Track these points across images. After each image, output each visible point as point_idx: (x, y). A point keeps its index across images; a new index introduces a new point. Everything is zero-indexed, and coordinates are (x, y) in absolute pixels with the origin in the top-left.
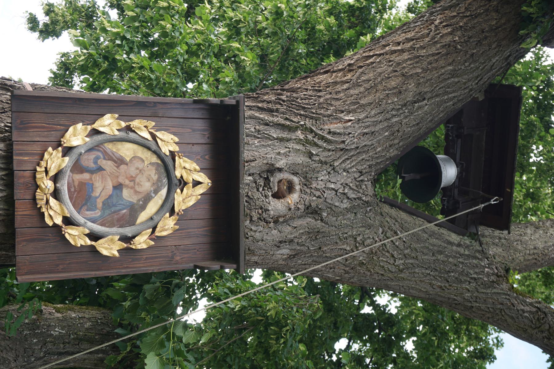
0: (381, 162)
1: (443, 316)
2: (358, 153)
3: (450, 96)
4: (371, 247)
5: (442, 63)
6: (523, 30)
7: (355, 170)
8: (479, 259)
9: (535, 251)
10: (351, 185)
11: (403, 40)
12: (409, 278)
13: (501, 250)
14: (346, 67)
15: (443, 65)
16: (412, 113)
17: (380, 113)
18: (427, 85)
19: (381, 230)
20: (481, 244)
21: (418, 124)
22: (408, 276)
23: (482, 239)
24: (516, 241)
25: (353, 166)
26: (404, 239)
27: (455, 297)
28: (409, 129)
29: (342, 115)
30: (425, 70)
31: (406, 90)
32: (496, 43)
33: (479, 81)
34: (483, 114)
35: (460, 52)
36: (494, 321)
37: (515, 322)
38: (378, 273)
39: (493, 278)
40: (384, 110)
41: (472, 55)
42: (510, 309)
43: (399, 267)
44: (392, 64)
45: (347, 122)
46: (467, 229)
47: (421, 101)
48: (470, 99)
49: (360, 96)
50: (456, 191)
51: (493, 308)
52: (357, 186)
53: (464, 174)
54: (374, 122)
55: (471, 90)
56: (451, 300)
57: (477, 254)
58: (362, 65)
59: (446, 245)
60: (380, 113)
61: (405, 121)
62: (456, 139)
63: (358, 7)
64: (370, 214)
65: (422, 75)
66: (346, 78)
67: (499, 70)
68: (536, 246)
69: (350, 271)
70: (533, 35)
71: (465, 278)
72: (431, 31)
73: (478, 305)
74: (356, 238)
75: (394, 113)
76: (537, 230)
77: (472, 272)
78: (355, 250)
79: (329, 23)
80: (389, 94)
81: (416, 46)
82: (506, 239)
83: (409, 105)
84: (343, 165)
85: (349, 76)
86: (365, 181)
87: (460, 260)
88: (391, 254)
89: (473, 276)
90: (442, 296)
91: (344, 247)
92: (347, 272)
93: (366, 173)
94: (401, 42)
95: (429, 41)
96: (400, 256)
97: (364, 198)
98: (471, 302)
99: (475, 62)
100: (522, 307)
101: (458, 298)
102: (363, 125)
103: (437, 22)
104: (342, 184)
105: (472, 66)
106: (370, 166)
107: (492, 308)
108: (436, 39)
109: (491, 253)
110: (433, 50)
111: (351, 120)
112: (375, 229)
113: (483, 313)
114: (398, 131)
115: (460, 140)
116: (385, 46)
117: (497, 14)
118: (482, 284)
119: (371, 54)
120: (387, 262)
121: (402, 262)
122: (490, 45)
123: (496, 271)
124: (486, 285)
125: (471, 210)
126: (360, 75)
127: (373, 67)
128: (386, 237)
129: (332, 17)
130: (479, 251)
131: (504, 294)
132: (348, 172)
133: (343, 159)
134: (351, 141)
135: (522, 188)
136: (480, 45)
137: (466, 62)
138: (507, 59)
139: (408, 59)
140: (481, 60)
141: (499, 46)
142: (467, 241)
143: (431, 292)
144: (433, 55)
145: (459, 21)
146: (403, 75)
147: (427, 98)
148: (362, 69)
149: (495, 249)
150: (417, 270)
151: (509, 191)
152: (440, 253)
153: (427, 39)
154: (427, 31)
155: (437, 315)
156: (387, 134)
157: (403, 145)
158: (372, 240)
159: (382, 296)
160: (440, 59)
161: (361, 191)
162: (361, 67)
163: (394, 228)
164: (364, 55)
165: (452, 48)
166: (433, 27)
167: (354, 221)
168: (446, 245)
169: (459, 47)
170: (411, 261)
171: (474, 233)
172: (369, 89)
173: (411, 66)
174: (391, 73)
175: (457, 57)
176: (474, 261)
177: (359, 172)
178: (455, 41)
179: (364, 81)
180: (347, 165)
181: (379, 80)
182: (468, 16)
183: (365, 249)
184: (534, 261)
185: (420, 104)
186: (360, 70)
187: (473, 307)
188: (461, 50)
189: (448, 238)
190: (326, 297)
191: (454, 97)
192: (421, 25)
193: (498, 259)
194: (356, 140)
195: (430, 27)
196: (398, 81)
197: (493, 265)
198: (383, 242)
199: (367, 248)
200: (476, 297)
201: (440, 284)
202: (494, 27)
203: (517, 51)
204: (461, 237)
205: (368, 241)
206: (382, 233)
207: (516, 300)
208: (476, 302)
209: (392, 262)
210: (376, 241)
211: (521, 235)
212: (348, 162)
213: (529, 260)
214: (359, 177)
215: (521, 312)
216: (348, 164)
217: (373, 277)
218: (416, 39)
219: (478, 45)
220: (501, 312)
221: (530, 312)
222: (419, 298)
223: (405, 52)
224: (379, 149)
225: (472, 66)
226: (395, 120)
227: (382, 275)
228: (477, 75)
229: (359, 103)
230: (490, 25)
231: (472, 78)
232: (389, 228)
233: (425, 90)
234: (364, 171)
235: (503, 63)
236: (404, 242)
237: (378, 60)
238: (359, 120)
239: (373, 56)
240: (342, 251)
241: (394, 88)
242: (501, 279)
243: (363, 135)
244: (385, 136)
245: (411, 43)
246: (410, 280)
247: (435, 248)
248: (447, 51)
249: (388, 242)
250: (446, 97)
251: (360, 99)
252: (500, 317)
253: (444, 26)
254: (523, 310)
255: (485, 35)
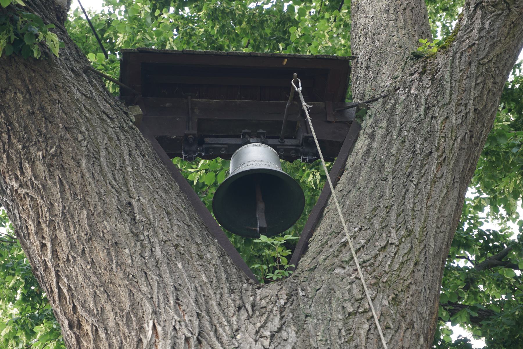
0: (226, 272)
1: (514, 146)
2: (208, 314)
3: (127, 162)
4: (365, 286)
5: (75, 177)
6: (33, 52)
7: (235, 318)
8: (395, 104)
9: (392, 11)
10: (258, 325)
11: (38, 239)
12: (423, 219)
13: (385, 67)
14: (75, 333)
15: (79, 175)
16: (150, 224)
17: (147, 277)
18: (107, 201)
19: (338, 271)
20: (374, 100)
21: (168, 214)
22: (420, 220)
23: (367, 98)
24: (374, 42)
25: (228, 322)
26: (356, 229)
27: (459, 140)
28: (175, 228)
29: (145, 342)
30: (85, 204)
31: (113, 235)
32: (51, 92)
33: (109, 117)
34: (167, 105)
35: (61, 148)
36: (501, 73)
37: (500, 40)
38: (413, 271)
39: (426, 80)
40: (142, 270)
41: (66, 129)
42: (478, 51)
43: (403, 237)
44: (73, 257)
45: (157, 333)
46: (351, 123)
47: (133, 209)
48: (137, 129)
49: (118, 311)
50: (288, 142)
51: (477, 78)
52: (262, 315)
53: (261, 131)
54: (159, 287)
55: (122, 129)
56: (464, 146)
57: (388, 106)
58: (71, 306)
59: (370, 159)
60: (147, 277)
61: (161, 236)
62: (204, 146)
63: (25, 287)
64: (309, 290)
65: (92, 208)
66: (90, 334)
67: (94, 86)
68: (383, 9)
69: (408, 320)
70: (41, 37)
71: (425, 126)
72: (27, 194)
73: (471, 102)
74: (350, 314)
75: (147, 254)
76: (361, 8)
77: (415, 115)
78: (370, 314)
79: (45, 335)
80: (117, 262)
81: (48, 218)
82: (370, 59)
83: (138, 228)
84: (225, 339)
85: (87, 328)
86: (254, 300)
87: (395, 134)
88: (380, 251)
89: (422, 113)
90: (457, 161)
91: (363, 333)
92: (411, 325)
93: (241, 298)
94: (41, 243)
95: (42, 198)
96: (384, 235)
97: (282, 302)
98: (466, 114)
99: (77, 124)
100: (476, 31)
101: (460, 134)
102: (162, 306)
103: (16, 185)
104: (256, 341)
105: (83, 129)
106: (232, 291)
107: (477, 79)
108: (40, 186)
109: (388, 83)
110: (55, 190)
111: (154, 325)
112: (336, 280)
113: (485, 92)
114: (176, 246)
115: (207, 140)
116: (46, 268)
117: (8, 91)
118: (437, 97)
119: (56, 290)
120: (393, 258)
121: (394, 231)
122: (54, 102)
123: (416, 75)
124: (439, 91)
125: (310, 122)
126: (86, 311)
127: (76, 288)
128: (350, 260)
129: (36, 329)
130: (385, 103)
131: (453, 61)
132: (237, 330)
133: (214, 339)
134: (186, 326)
135: (323, 17)
136: (53, 117)
137: (76, 139)
138: (77, 75)
139: (66, 231)
140: (75, 115)
141: (56, 88)
142: (368, 122)
143: (449, 180)
144: (62, 191)
145: (16, 150)
146: (90, 239)
147: (128, 200)
148: (78, 306)
149: (384, 77)
150: (409, 206)
151: (286, 60)
152: (381, 167)
153: (39, 200)
154: (28, 200)
155: (513, 154)
156: (180, 265)
157: (203, 237)
158: (354, 285)
159: (510, 231)
160: (70, 180)
161: (270, 307)
162: (74, 308)
163: (336, 248)
164: (57, 302)
165: (54, 162)
166: (22, 191)
167: (320, 317)
168: (370, 159)
169: (53, 150)
170: (393, 218)
171: (356, 112)
172: (108, 296)
173: (77, 226)
174: (85, 259)
175: (68, 154)
176: (398, 111)
177: (238, 311)
178: (43, 157)
179: (95, 303)
180: (225, 332)
181: (95, 279)
182: (9, 136)
183: (369, 297)
184: (407, 11)
185: (136, 211)
186: (79, 309)
187: (475, 110)
188: (59, 147)
189: (360, 155)
190: (505, 330)
191: (130, 155)
192: (18, 209)
193: (399, 72)
194: (186, 318)
195: (22, 196)
196: (98, 248)
197: (405, 81)
198: (358, 266)
199: (367, 292)
200: (458, 105)
201: (434, 167)
202: (27, 96)
203: (67, 59)
204: (362, 131)
205: (356, 292)
206: (344, 268)
207: (464, 41)
208: (466, 105)
209: (393, 249)
210: (356, 278)
211: (366, 34)
212: (220, 330)
213: (405, 20)
214: (247, 310)
215: (483, 33)
216: (224, 330)
217: (420, 279)
218: (38, 217)
219: (51, 119)
220: (484, 64)
221: (482, 18)
222: (461, 197)
223: (56, 236)
224: (204, 278)
225: (83, 129)
226: (158, 252)
227: (416, 264)
228: (98, 121)
229: (128, 313)
230: (23, 102)
231: (103, 127)
232: (337, 256)
233: (115, 202)
234: (238, 302)
235: (84, 80)
236: (361, 229)
237: (65, 280)
238: (154, 312)
239: (59, 288)
240: (371, 336)
241: (109, 253)
242: (429, 67)
243: (179, 305)
244: (184, 267)
245: (43, 225)
246: (427, 217)
247: (374, 177)
248: (57, 168)
249: (359, 258)
250: (129, 169)
251: (123, 311)
252: (491, 65)
253: (22, 173)
254: (480, 30)
255: (38, 109)
